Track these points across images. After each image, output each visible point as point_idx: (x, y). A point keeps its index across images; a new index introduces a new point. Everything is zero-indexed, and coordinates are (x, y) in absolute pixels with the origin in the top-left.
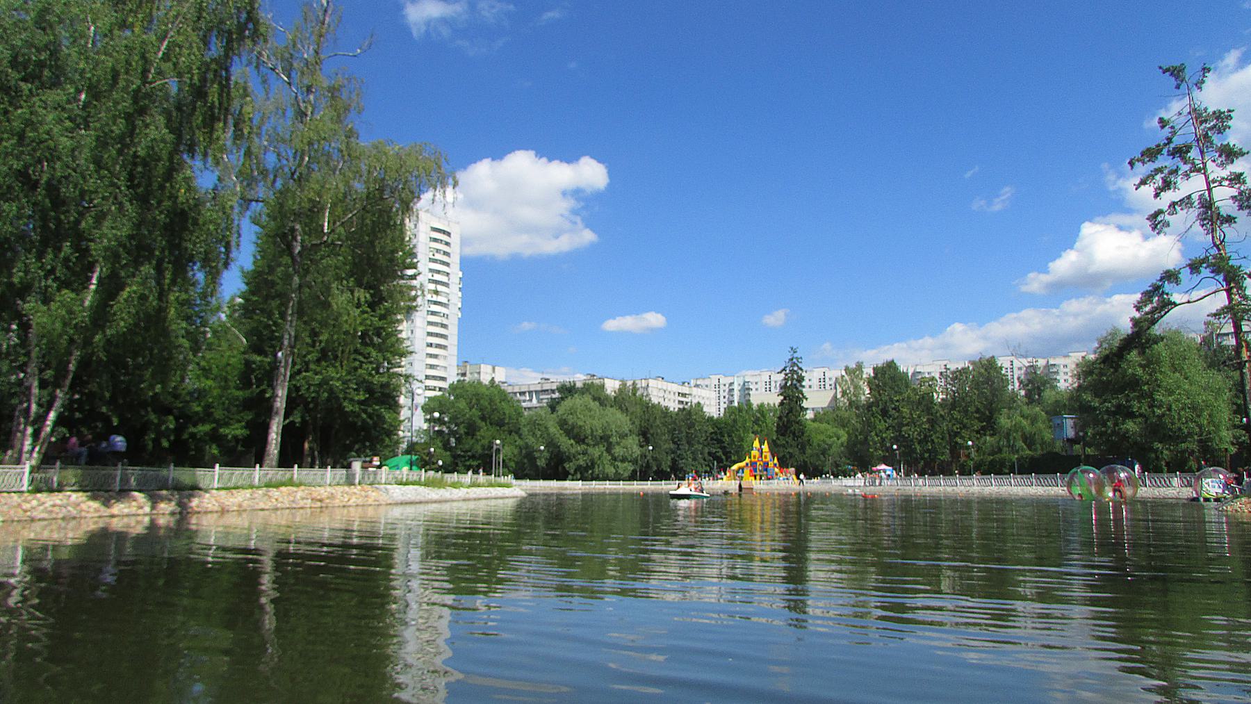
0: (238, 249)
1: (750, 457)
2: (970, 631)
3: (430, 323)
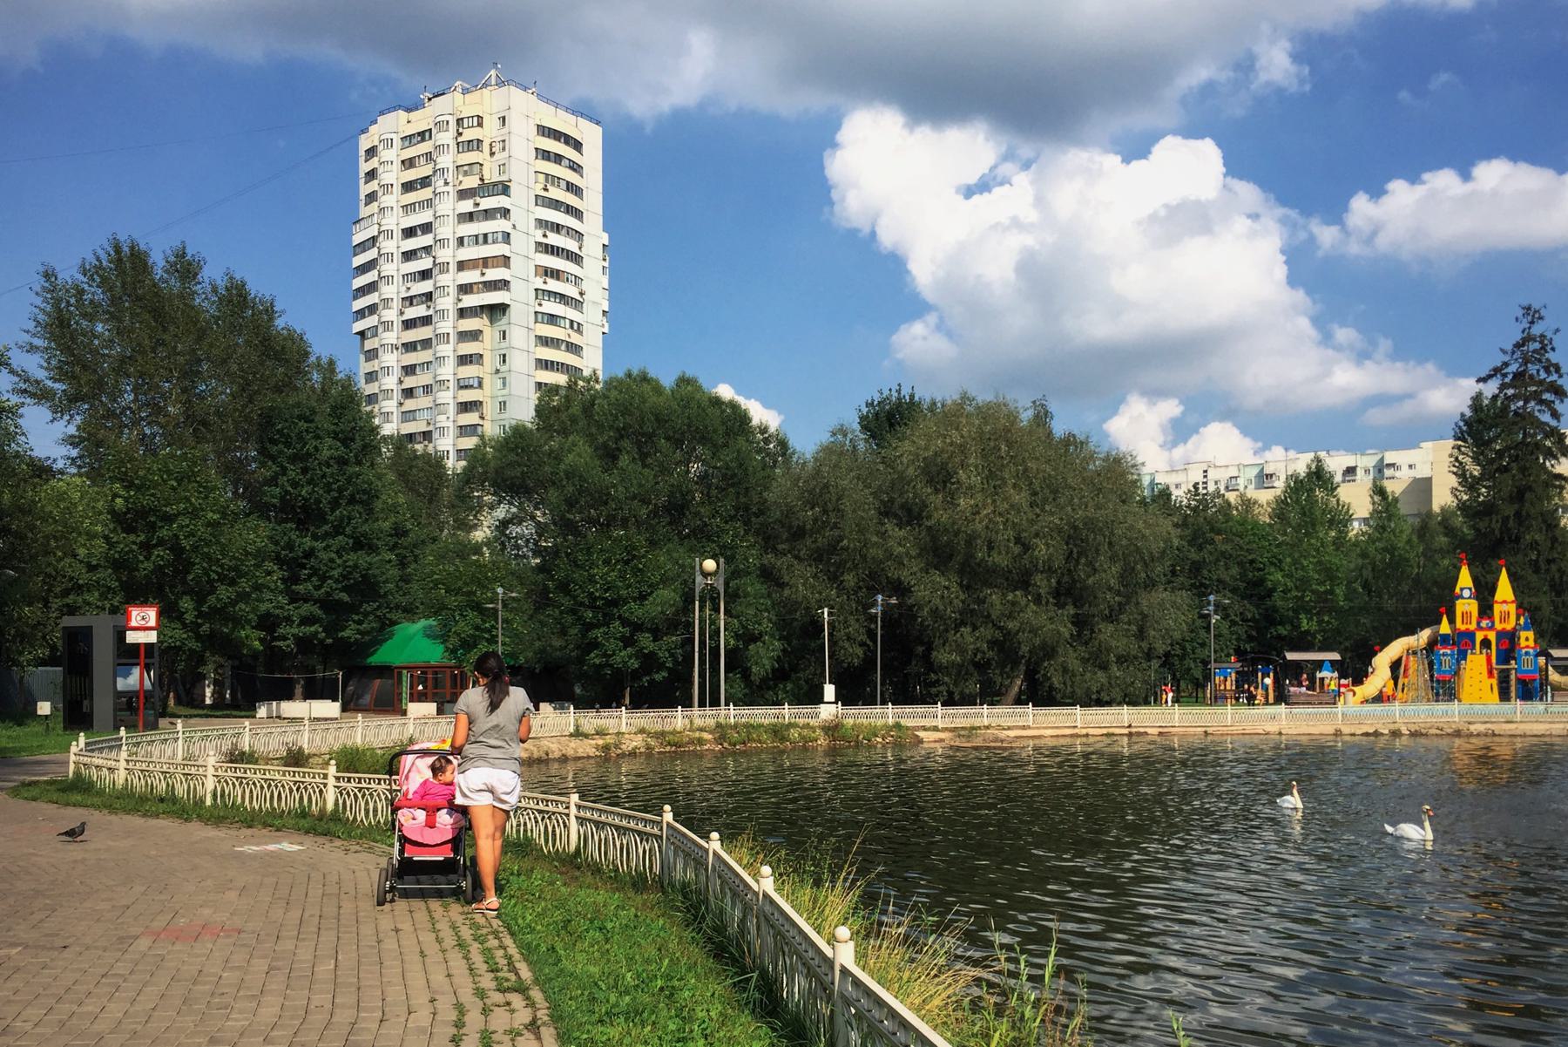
0: (58, 790)
1: (1452, 621)
2: (1548, 726)
3: (545, 341)
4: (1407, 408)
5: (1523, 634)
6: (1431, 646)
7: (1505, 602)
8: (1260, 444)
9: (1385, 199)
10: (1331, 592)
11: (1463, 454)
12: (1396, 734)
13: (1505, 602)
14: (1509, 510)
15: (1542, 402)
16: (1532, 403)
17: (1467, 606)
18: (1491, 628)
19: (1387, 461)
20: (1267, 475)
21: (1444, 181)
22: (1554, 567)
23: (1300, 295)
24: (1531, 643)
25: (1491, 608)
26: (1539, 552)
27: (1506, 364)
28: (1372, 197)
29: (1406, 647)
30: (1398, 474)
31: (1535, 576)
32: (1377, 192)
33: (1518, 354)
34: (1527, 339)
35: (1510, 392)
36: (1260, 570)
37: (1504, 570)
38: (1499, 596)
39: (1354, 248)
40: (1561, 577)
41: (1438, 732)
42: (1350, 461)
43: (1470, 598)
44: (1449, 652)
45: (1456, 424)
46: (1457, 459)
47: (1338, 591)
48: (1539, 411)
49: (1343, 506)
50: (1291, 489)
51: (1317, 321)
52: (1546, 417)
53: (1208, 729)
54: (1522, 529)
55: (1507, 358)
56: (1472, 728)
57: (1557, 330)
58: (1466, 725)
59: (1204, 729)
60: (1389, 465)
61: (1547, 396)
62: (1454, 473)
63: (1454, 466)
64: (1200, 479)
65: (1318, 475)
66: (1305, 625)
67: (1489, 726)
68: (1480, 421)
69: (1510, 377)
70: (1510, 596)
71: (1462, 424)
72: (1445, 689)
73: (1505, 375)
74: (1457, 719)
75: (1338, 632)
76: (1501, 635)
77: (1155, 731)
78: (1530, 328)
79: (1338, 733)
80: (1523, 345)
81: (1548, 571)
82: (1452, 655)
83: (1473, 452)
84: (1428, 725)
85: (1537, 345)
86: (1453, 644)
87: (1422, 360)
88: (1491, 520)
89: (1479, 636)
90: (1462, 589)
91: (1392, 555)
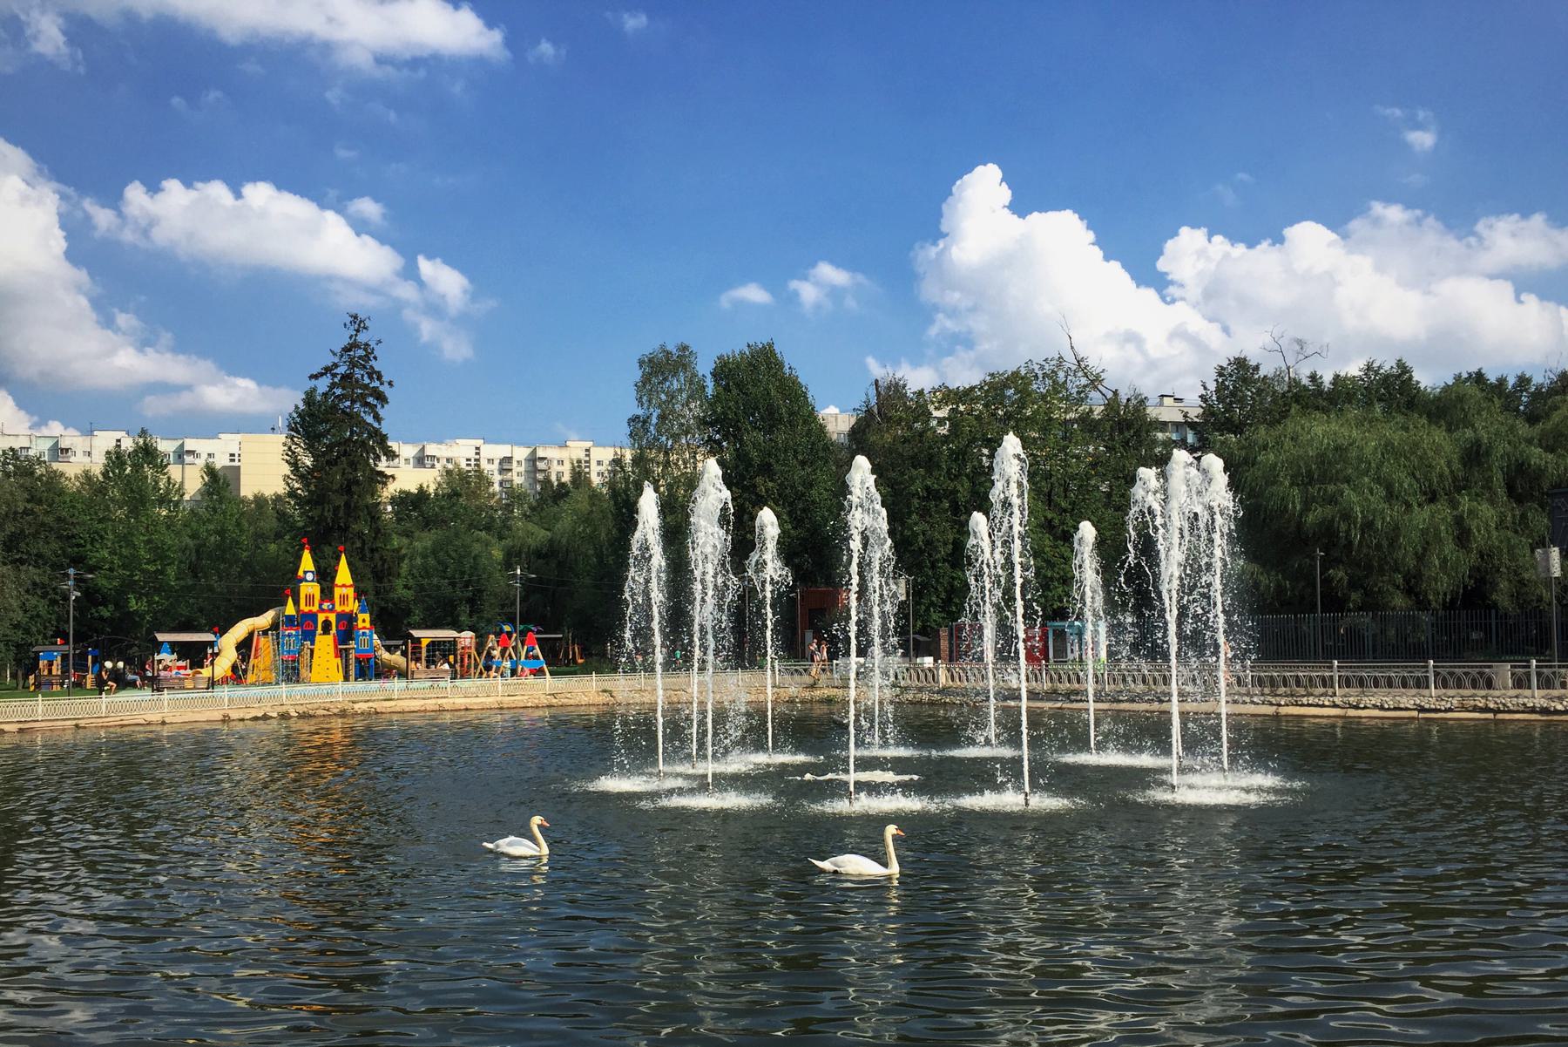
1: (296, 603)
2: (423, 702)
4: (185, 400)
5: (361, 616)
6: (275, 626)
7: (344, 586)
8: (36, 419)
9: (160, 196)
10: (162, 572)
11: (296, 444)
12: (284, 716)
13: (344, 586)
14: (340, 501)
15: (367, 404)
16: (357, 405)
17: (310, 588)
18: (331, 610)
19: (186, 448)
20: (62, 450)
21: (218, 191)
22: (377, 556)
23: (82, 276)
24: (367, 625)
25: (332, 592)
26: (364, 541)
27: (336, 365)
28: (148, 191)
29: (251, 628)
30: (197, 461)
31: (361, 563)
32: (154, 188)
33: (345, 358)
34: (353, 346)
35: (338, 391)
36: (79, 545)
37: (343, 557)
38: (338, 581)
39: (128, 236)
40: (383, 565)
41: (326, 712)
42: (502, 451)
43: (312, 581)
44: (294, 633)
45: (290, 414)
46: (290, 449)
47: (169, 572)
48: (365, 412)
49: (174, 485)
50: (113, 463)
51: (97, 304)
52: (369, 419)
53: (80, 722)
54: (350, 519)
55: (336, 360)
56: (356, 706)
57: (380, 342)
58: (351, 704)
59: (74, 722)
60: (189, 452)
61: (370, 400)
62: (287, 461)
63: (287, 455)
64: (582, 455)
65: (147, 453)
66: (133, 605)
67: (370, 704)
68: (311, 415)
69: (339, 377)
70: (349, 581)
71: (295, 415)
72: (292, 672)
73: (334, 375)
74: (341, 699)
75: (166, 612)
76: (340, 616)
77: (13, 728)
78: (356, 335)
79: (226, 720)
80: (350, 350)
81: (372, 559)
82: (297, 636)
83: (305, 444)
84: (316, 706)
85: (361, 352)
86: (298, 625)
87: (202, 354)
88: (323, 509)
89: (321, 617)
90: (305, 572)
91: (223, 539)
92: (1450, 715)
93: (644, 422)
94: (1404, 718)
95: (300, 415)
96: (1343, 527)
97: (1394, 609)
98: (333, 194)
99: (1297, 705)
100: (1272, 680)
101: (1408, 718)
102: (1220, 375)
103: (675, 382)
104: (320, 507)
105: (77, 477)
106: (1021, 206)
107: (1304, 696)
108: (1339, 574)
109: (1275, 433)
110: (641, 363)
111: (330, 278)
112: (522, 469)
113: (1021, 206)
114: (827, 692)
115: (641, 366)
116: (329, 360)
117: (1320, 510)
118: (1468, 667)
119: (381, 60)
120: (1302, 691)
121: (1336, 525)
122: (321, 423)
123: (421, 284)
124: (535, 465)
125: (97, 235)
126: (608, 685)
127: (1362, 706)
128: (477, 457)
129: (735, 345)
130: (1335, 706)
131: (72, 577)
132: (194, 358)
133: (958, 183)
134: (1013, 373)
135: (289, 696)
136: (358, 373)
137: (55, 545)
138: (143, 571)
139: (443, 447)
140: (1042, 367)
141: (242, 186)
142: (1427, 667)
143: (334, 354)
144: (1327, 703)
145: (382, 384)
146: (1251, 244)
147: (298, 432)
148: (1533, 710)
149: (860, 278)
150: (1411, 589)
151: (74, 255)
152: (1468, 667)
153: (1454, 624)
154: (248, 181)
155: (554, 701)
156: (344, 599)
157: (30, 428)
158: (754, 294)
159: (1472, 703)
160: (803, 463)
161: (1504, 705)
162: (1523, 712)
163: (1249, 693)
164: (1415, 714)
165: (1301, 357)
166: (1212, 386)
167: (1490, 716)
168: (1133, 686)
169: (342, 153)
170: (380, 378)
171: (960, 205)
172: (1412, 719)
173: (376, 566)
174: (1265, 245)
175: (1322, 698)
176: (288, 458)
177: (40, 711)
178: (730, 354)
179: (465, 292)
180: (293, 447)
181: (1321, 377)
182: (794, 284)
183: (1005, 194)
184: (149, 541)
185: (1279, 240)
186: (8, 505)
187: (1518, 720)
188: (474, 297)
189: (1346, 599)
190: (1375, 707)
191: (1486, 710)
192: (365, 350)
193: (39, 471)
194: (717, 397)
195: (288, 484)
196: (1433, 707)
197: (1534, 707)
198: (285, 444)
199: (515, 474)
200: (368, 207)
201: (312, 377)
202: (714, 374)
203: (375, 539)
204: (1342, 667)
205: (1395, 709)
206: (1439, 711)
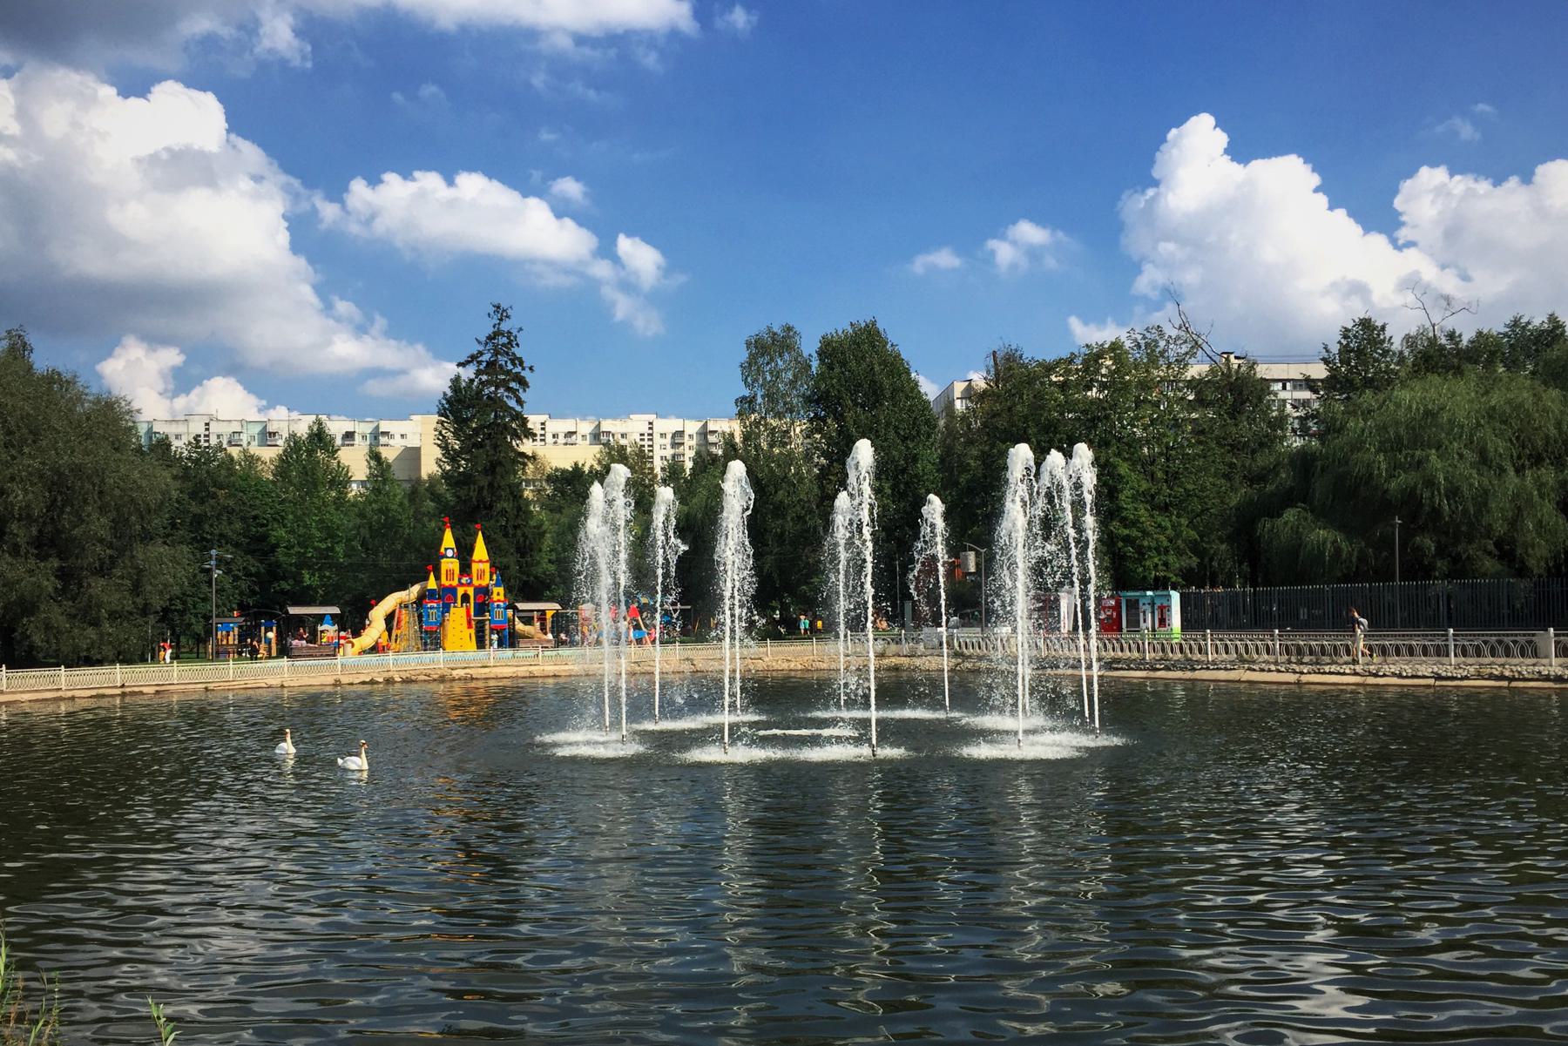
1: (438, 578)
4: (402, 383)
5: (496, 590)
7: (480, 561)
8: (264, 403)
9: (381, 188)
10: (332, 549)
13: (480, 561)
14: (484, 481)
16: (501, 390)
17: (450, 564)
18: (470, 584)
19: (381, 430)
20: (270, 433)
21: (430, 181)
22: (519, 532)
24: (502, 598)
25: (470, 567)
27: (481, 353)
29: (399, 601)
32: (374, 181)
33: (490, 346)
35: (484, 378)
36: (263, 525)
39: (354, 228)
40: (525, 541)
41: (427, 678)
43: (452, 557)
44: (435, 605)
46: (440, 433)
48: (507, 397)
51: (319, 290)
52: (512, 403)
56: (455, 673)
57: (521, 329)
59: (204, 686)
60: (385, 434)
61: (513, 385)
62: (439, 445)
65: (319, 437)
67: (467, 671)
69: (484, 364)
70: (486, 557)
71: (444, 402)
73: (480, 363)
77: (151, 690)
79: (337, 683)
80: (494, 338)
81: (514, 535)
84: (418, 672)
85: (505, 340)
86: (439, 598)
89: (461, 591)
90: (446, 549)
92: (1466, 683)
93: (750, 402)
94: (1420, 686)
95: (448, 402)
96: (1426, 494)
97: (1484, 575)
98: (537, 175)
99: (1319, 673)
100: (1300, 651)
101: (1424, 686)
102: (1345, 337)
103: (780, 363)
104: (466, 487)
105: (271, 461)
106: (1240, 151)
107: (1328, 664)
108: (1428, 543)
109: (1381, 397)
110: (748, 344)
111: (533, 261)
112: (693, 442)
113: (1240, 151)
114: (894, 661)
115: (748, 348)
116: (475, 348)
117: (1403, 476)
118: (1487, 635)
119: (581, 39)
120: (1326, 659)
121: (1418, 492)
122: (468, 408)
123: (616, 260)
124: (706, 438)
125: (323, 227)
126: (690, 654)
127: (1381, 674)
128: (651, 432)
129: (839, 323)
130: (1356, 674)
131: (214, 558)
132: (404, 342)
133: (1174, 131)
134: (1113, 343)
135: (434, 661)
136: (502, 360)
137: (238, 526)
138: (315, 549)
139: (618, 422)
140: (1144, 337)
141: (457, 174)
142: (1447, 635)
143: (479, 342)
144: (1348, 671)
145: (523, 369)
146: (1498, 181)
147: (447, 417)
148: (1547, 678)
149: (1060, 234)
150: (1507, 552)
151: (296, 247)
152: (1487, 635)
153: (1544, 592)
154: (463, 170)
155: (638, 668)
156: (481, 575)
157: (260, 411)
158: (945, 259)
159: (1488, 671)
160: (904, 439)
161: (1519, 673)
162: (1537, 680)
163: (1277, 662)
164: (1431, 681)
165: (1448, 313)
166: (1335, 349)
167: (1505, 684)
168: (1171, 655)
169: (546, 136)
170: (521, 363)
171: (1175, 152)
172: (1428, 686)
173: (518, 542)
174: (1513, 182)
175: (1344, 667)
176: (439, 442)
177: (175, 675)
178: (833, 332)
179: (659, 268)
180: (444, 432)
181: (1460, 336)
182: (993, 244)
183: (1222, 139)
184: (322, 521)
185: (1527, 178)
186: (163, 494)
187: (1532, 688)
188: (667, 271)
189: (1432, 567)
190: (1394, 675)
191: (1502, 677)
192: (508, 338)
193: (220, 455)
194: (821, 376)
195: (440, 466)
196: (1449, 674)
197: (1549, 675)
198: (436, 430)
199: (687, 447)
200: (570, 187)
201: (459, 365)
202: (819, 354)
203: (517, 516)
204: (1458, 635)
205: (1413, 677)
206: (1453, 678)
